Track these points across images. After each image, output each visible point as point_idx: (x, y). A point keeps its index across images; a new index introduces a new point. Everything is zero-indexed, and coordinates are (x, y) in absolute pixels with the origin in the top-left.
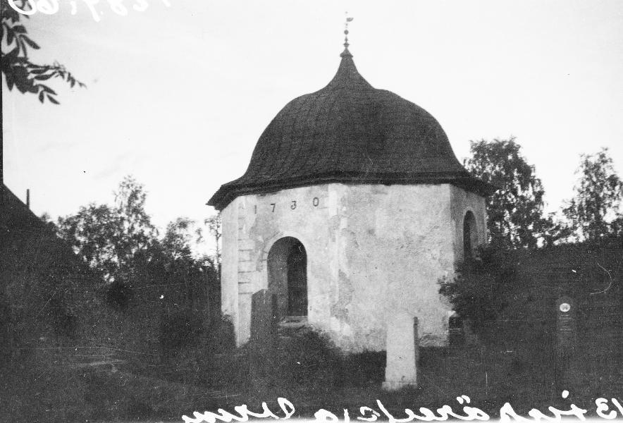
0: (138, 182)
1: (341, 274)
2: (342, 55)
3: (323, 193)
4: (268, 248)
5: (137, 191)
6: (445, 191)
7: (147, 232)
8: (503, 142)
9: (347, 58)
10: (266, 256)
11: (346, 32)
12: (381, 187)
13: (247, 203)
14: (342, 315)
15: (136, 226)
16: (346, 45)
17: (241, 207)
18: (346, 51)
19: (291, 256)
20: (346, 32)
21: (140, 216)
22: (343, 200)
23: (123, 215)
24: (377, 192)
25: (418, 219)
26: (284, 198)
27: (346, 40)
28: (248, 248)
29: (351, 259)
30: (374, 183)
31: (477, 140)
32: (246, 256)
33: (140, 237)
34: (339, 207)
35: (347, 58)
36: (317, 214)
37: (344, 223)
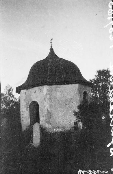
0: (11, 86)
1: (48, 110)
3: (43, 88)
5: (11, 89)
6: (77, 86)
7: (14, 99)
8: (106, 70)
9: (52, 49)
11: (51, 43)
14: (49, 123)
15: (11, 98)
16: (51, 46)
18: (51, 48)
19: (34, 107)
20: (51, 43)
21: (11, 95)
23: (7, 95)
24: (57, 87)
25: (70, 92)
26: (32, 90)
27: (51, 45)
28: (24, 104)
29: (51, 106)
30: (57, 84)
31: (99, 69)
33: (12, 101)
35: (52, 49)
36: (40, 94)
37: (48, 96)
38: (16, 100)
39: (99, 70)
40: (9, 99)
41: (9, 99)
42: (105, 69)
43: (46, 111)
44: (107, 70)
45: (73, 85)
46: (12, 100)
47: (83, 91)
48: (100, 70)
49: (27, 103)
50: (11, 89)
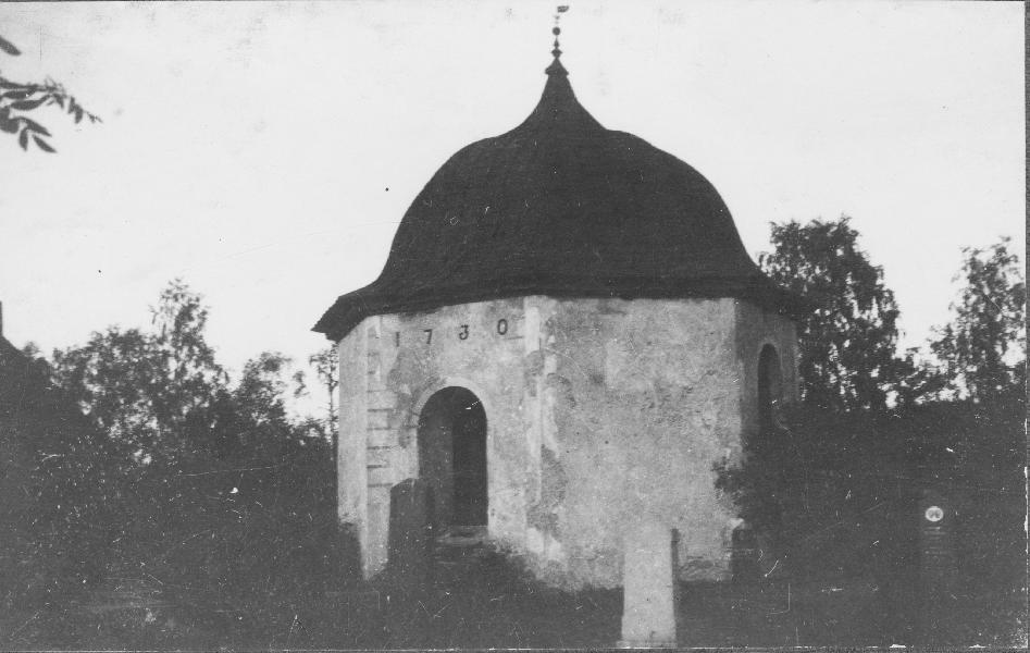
0: (193, 291)
1: (546, 454)
2: (549, 71)
3: (515, 311)
4: (419, 406)
6: (726, 311)
7: (208, 376)
8: (829, 226)
9: (557, 74)
10: (415, 420)
11: (557, 31)
12: (615, 303)
13: (382, 325)
14: (548, 525)
15: (190, 367)
16: (557, 53)
17: (372, 335)
18: (557, 63)
19: (454, 427)
20: (557, 31)
21: (196, 349)
22: (550, 326)
23: (167, 346)
24: (608, 311)
25: (678, 348)
26: (447, 321)
27: (557, 44)
31: (783, 220)
32: (381, 421)
33: (197, 385)
34: (543, 336)
35: (557, 74)
36: (499, 351)
37: (551, 364)
38: (222, 381)
39: (789, 222)
40: (182, 372)
41: (182, 372)
42: (824, 221)
43: (534, 451)
44: (842, 228)
45: (706, 303)
46: (201, 375)
47: (762, 344)
48: (856, 233)
49: (401, 397)
50: (192, 307)
